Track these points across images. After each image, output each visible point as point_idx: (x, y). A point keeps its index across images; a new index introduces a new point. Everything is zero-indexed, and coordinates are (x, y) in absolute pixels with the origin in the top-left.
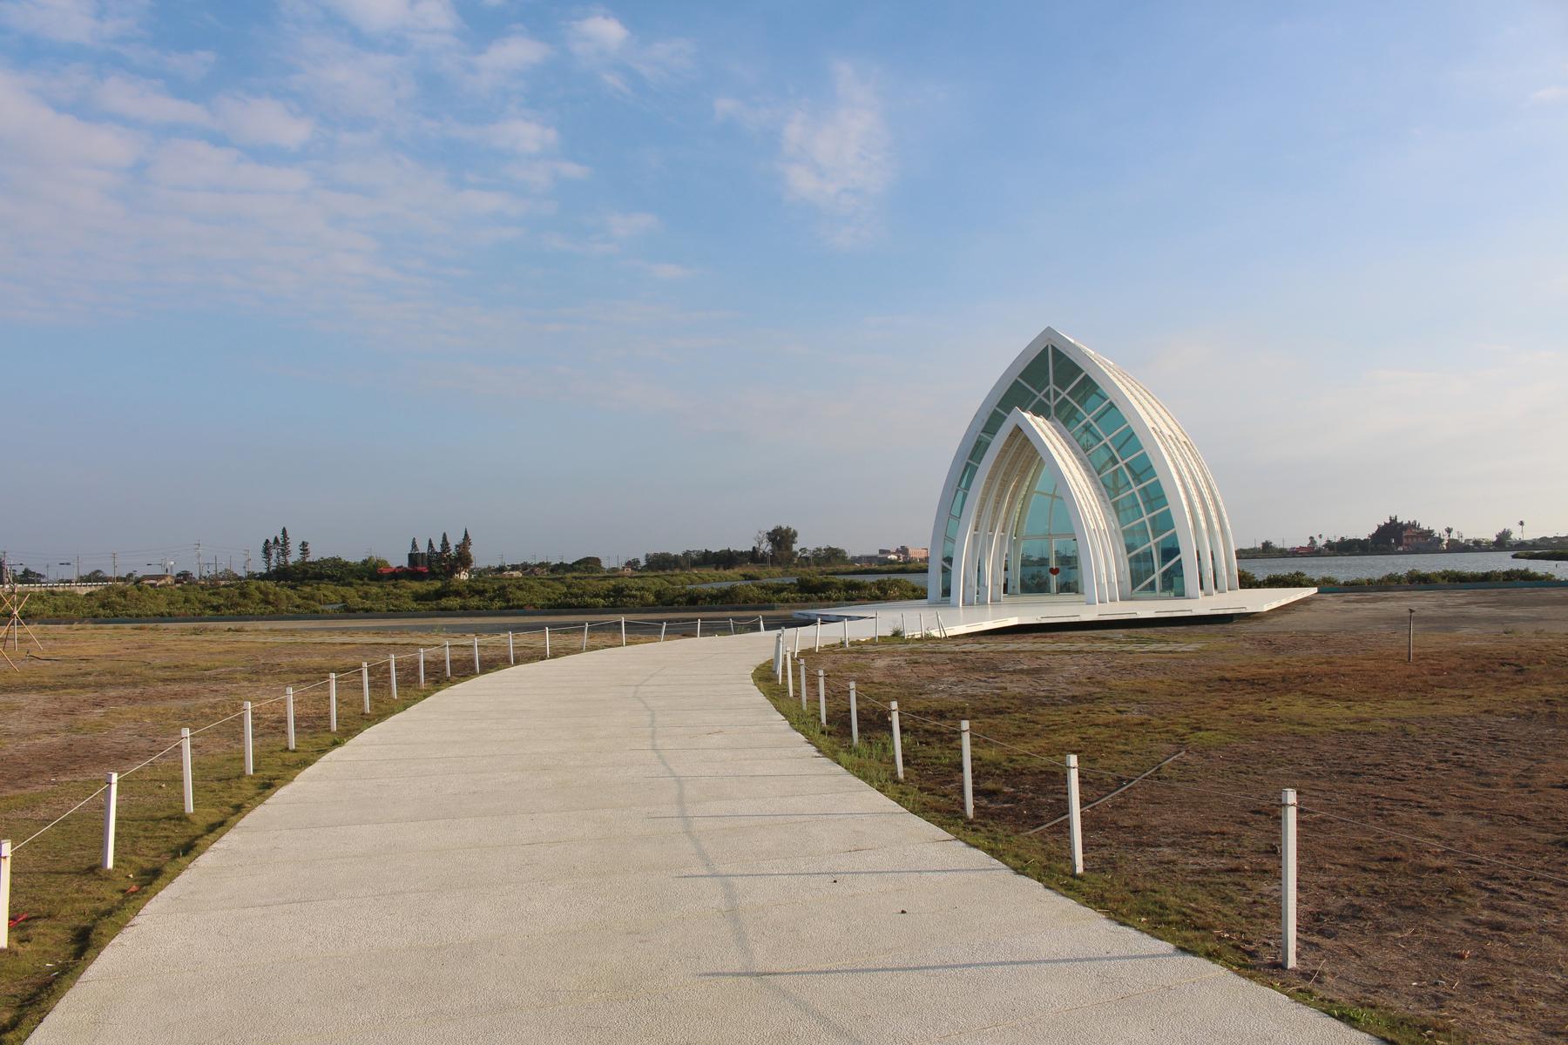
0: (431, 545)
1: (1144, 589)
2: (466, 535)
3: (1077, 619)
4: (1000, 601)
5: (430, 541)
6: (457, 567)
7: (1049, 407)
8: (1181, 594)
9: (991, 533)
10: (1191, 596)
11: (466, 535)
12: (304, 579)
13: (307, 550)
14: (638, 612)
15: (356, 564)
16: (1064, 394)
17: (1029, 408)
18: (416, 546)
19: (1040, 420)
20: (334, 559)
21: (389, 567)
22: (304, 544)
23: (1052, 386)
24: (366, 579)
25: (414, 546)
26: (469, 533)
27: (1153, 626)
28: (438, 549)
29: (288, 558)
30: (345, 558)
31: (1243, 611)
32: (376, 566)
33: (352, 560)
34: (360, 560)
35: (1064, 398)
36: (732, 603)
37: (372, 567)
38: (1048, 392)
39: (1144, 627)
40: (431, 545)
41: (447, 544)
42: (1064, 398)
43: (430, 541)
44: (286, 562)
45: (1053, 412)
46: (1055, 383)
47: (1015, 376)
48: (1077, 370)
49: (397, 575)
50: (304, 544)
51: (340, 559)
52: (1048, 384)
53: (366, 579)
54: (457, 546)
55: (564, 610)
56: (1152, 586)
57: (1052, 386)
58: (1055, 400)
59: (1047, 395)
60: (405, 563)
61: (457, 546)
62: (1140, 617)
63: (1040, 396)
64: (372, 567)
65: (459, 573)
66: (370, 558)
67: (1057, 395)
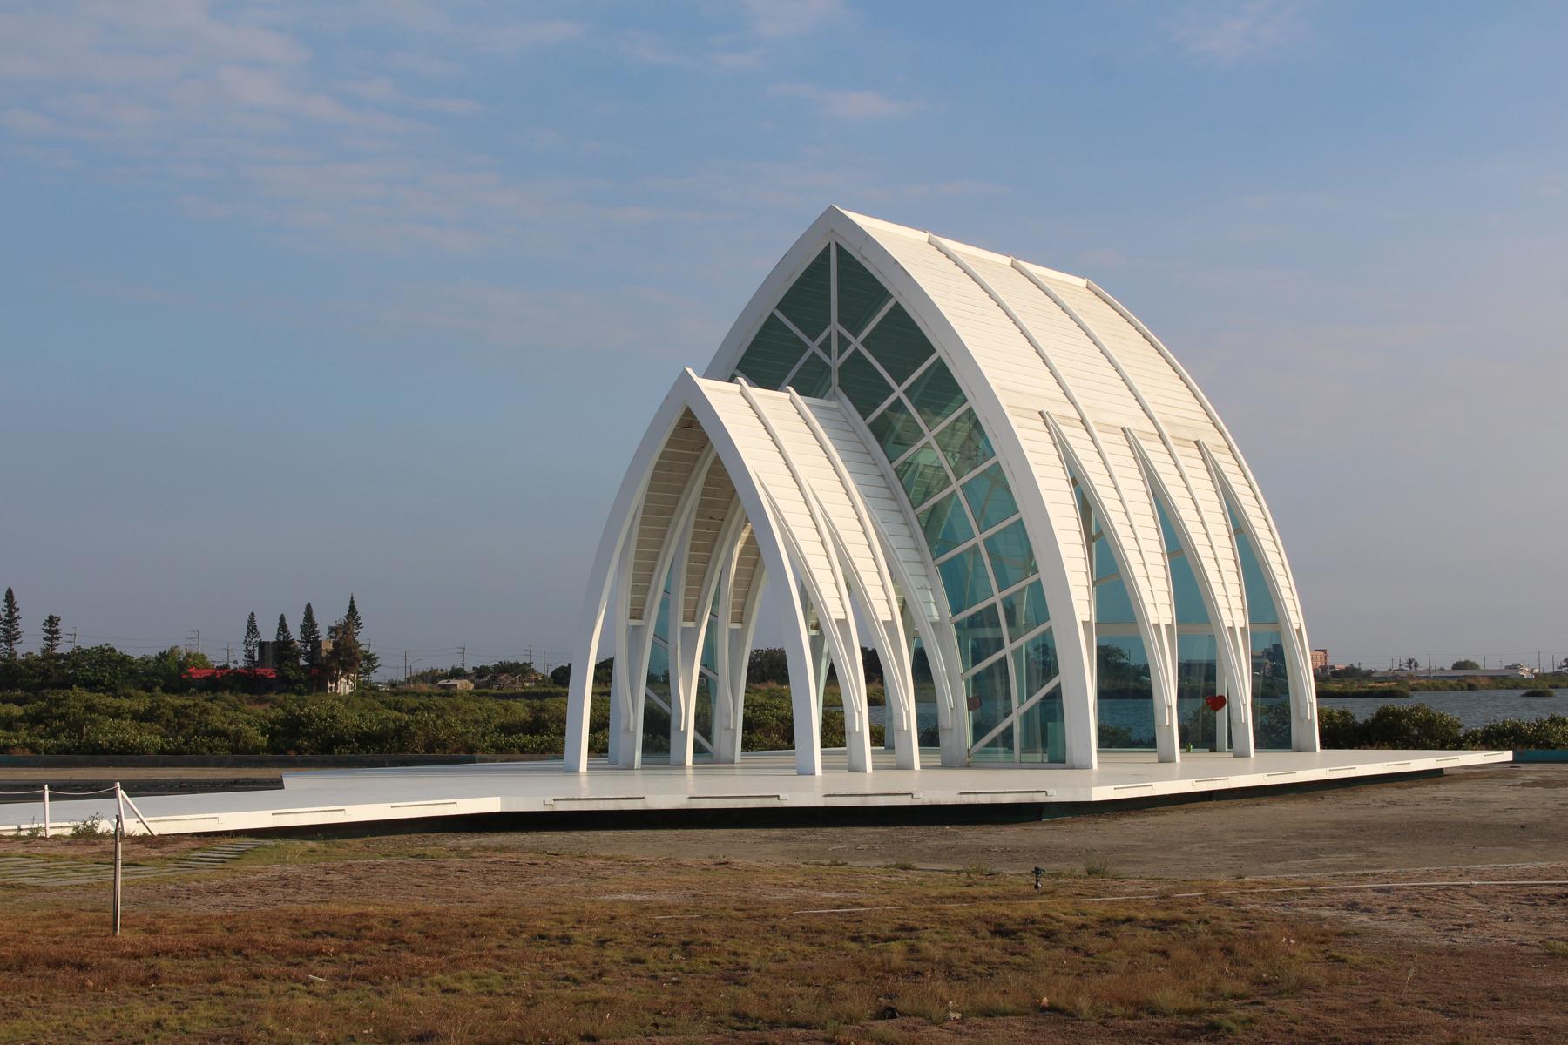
0: (283, 626)
1: (993, 743)
2: (352, 608)
3: (637, 805)
4: (733, 762)
5: (282, 619)
6: (332, 669)
7: (826, 368)
8: (1058, 759)
9: (691, 624)
10: (1076, 763)
11: (352, 608)
12: (42, 686)
13: (57, 632)
14: (220, 764)
15: (145, 661)
16: (856, 343)
17: (788, 379)
18: (255, 628)
19: (780, 405)
20: (101, 650)
21: (207, 666)
22: (52, 621)
23: (835, 327)
24: (158, 689)
25: (252, 628)
26: (356, 604)
27: (943, 823)
28: (295, 633)
29: (14, 647)
30: (123, 648)
31: (1040, 798)
32: (182, 666)
33: (136, 655)
34: (153, 653)
35: (863, 343)
36: (400, 750)
37: (174, 667)
38: (829, 338)
39: (546, 830)
40: (283, 626)
41: (314, 625)
42: (863, 343)
43: (282, 619)
44: (12, 654)
45: (835, 379)
46: (841, 321)
47: (769, 307)
48: (882, 294)
49: (220, 682)
50: (52, 621)
51: (113, 650)
52: (828, 323)
53: (158, 689)
54: (332, 629)
55: (82, 758)
56: (1007, 736)
57: (835, 327)
58: (840, 354)
59: (825, 346)
60: (238, 660)
61: (332, 629)
62: (787, 805)
63: (814, 346)
64: (174, 667)
65: (335, 680)
66: (172, 650)
67: (844, 343)
